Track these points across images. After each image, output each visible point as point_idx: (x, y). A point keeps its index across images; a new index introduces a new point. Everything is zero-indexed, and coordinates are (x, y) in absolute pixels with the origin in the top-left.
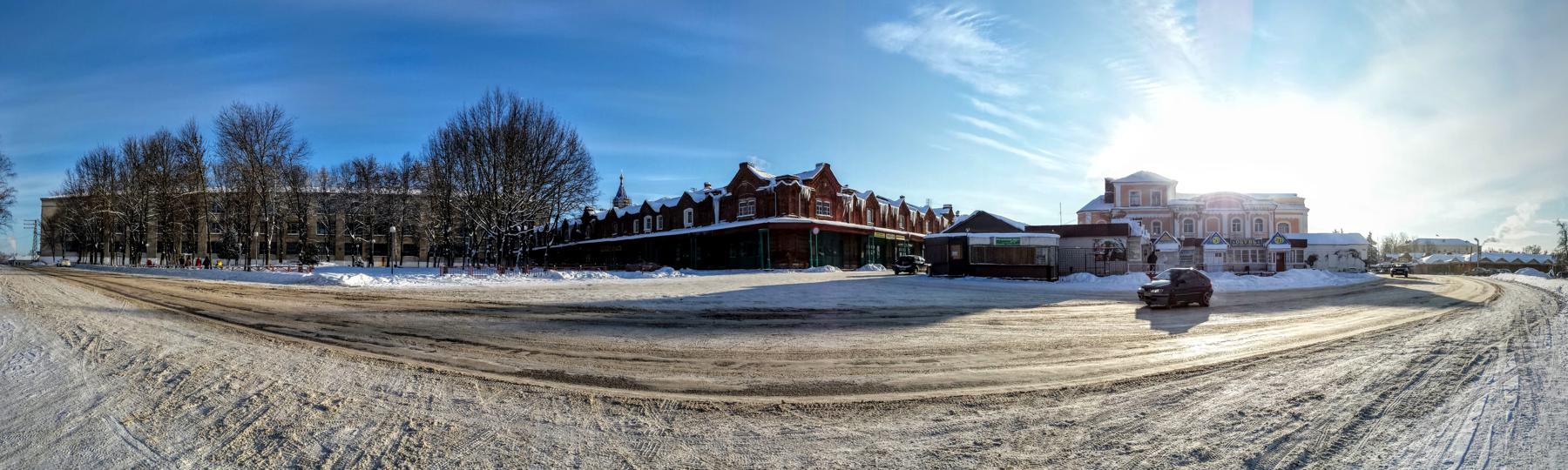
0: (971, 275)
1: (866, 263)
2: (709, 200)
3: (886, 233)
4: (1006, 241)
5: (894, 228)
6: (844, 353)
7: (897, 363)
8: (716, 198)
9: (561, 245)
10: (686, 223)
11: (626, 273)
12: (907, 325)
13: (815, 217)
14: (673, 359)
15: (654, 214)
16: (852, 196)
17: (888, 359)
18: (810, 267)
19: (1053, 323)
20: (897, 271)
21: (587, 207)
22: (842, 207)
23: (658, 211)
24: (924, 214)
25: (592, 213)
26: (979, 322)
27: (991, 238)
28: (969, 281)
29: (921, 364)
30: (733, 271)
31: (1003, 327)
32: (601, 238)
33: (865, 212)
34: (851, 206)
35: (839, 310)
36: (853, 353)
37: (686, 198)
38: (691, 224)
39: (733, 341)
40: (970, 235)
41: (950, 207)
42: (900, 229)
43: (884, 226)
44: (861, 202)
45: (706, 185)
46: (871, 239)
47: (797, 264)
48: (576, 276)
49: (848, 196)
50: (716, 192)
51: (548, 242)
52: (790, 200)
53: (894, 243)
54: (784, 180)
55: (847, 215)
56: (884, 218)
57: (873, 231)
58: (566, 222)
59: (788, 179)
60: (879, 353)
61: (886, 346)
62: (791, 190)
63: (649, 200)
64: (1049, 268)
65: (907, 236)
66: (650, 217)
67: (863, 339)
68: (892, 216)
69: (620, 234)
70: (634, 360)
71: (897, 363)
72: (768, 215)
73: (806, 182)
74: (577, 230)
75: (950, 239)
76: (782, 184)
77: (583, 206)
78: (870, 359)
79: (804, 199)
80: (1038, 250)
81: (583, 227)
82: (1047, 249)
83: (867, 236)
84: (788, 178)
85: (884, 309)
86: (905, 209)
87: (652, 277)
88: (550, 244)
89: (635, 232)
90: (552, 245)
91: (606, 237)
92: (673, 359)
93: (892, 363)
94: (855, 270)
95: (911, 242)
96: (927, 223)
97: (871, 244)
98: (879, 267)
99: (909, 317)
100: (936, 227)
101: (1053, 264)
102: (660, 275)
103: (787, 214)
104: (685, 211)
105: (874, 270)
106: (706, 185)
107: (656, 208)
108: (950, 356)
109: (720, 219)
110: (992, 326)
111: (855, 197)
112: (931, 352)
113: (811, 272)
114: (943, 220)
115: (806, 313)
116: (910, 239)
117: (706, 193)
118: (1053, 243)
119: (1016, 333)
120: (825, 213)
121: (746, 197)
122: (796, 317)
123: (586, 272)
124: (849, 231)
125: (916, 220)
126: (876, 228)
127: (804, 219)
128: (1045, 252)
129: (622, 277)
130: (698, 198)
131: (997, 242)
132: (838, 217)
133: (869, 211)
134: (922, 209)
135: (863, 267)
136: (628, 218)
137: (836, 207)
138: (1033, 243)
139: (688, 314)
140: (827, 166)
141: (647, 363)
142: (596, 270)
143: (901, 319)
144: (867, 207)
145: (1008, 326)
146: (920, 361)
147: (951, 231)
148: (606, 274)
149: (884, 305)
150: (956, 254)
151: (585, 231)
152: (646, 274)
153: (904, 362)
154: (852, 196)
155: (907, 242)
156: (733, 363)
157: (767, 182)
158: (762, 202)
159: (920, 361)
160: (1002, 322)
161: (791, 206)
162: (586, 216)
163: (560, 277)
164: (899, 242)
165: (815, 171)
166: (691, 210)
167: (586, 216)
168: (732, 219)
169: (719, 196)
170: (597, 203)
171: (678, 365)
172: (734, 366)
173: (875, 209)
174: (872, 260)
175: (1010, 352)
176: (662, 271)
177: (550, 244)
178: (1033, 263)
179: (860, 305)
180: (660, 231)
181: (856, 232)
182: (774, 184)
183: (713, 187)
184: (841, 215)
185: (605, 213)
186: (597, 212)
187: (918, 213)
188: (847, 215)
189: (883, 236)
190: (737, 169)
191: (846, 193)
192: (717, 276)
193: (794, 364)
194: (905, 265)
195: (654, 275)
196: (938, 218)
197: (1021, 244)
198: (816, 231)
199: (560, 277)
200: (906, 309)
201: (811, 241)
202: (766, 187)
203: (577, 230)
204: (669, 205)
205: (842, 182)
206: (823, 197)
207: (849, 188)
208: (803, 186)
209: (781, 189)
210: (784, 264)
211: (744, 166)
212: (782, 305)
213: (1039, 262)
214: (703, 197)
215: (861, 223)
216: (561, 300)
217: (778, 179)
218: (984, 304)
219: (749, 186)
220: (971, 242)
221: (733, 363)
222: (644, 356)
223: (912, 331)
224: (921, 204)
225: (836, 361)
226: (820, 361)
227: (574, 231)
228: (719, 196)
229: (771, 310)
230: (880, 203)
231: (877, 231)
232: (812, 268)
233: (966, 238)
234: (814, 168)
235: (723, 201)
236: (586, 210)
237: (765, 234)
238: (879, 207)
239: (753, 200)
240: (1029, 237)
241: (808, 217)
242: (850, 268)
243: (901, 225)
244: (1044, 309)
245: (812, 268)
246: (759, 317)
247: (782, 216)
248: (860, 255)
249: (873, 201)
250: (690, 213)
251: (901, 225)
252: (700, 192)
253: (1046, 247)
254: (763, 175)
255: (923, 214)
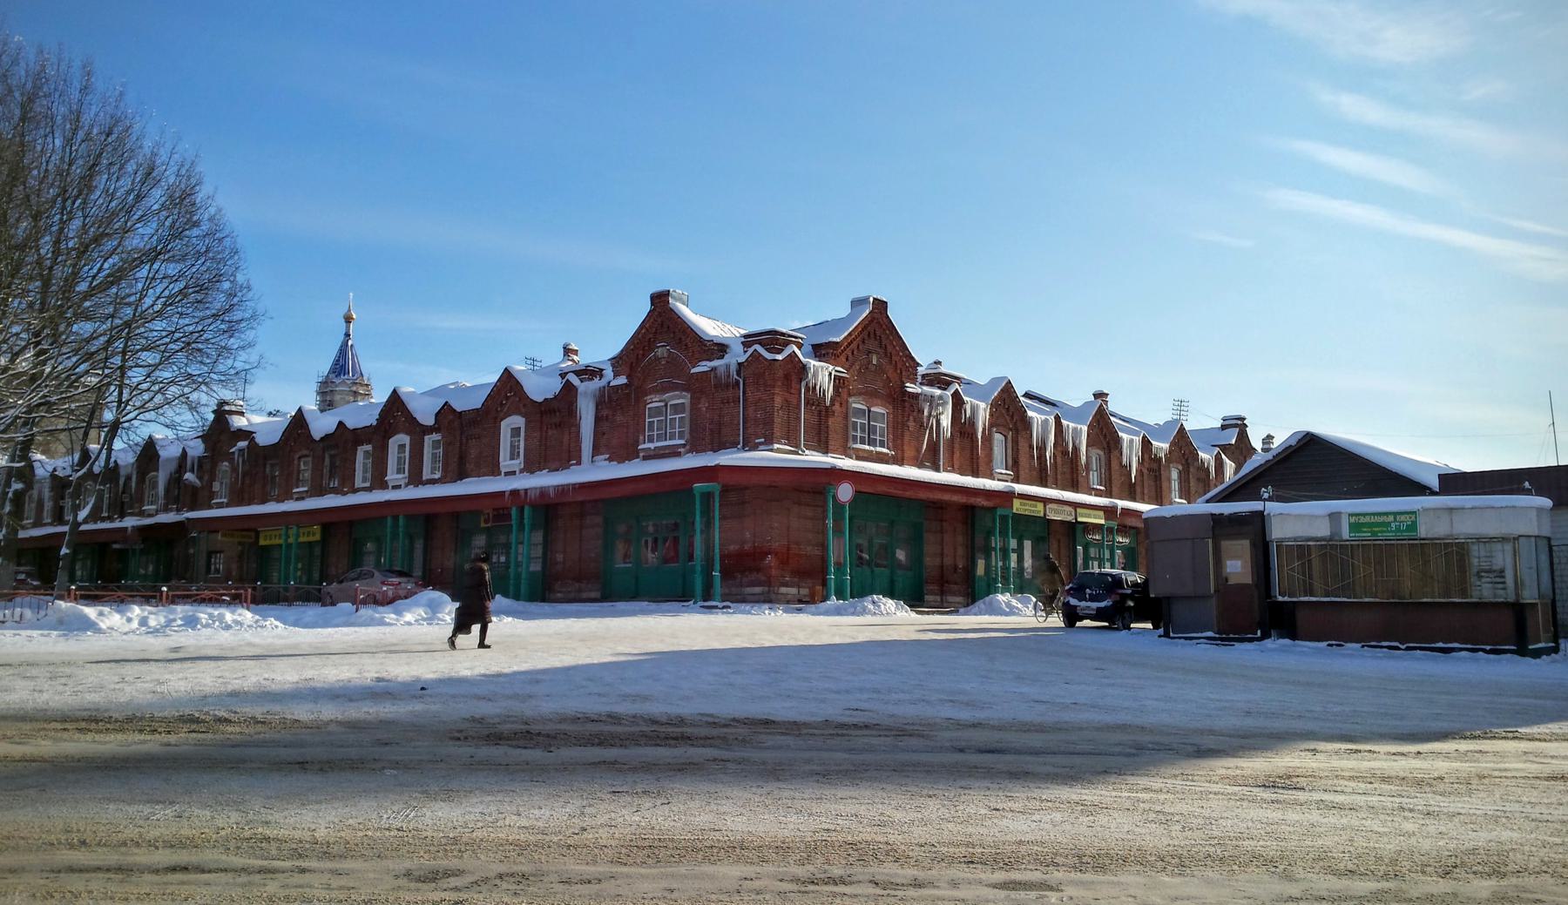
0: (1281, 636)
1: (990, 589)
2: (568, 390)
3: (1045, 501)
4: (1379, 521)
5: (1075, 487)
6: (783, 849)
7: (931, 884)
8: (587, 391)
9: (130, 522)
10: (506, 463)
11: (313, 611)
12: (1020, 775)
13: (846, 452)
14: (288, 864)
15: (418, 431)
16: (949, 393)
17: (910, 872)
18: (825, 598)
19: (1470, 793)
20: (1071, 617)
21: (222, 403)
22: (922, 427)
23: (428, 420)
24: (1165, 446)
25: (239, 422)
26: (1234, 781)
27: (1334, 517)
28: (1275, 654)
29: (1002, 894)
30: (621, 605)
31: (1302, 796)
32: (264, 502)
33: (988, 439)
34: (946, 421)
35: (842, 726)
36: (812, 850)
37: (508, 387)
38: (518, 464)
39: (493, 808)
40: (1273, 508)
41: (1237, 424)
42: (1090, 491)
43: (1043, 483)
44: (974, 409)
45: (567, 351)
46: (1004, 518)
47: (793, 591)
48: (143, 622)
49: (938, 392)
50: (589, 373)
51: (76, 509)
52: (778, 400)
53: (1073, 530)
54: (760, 343)
55: (934, 448)
56: (1042, 457)
57: (1009, 496)
58: (149, 451)
59: (776, 341)
60: (895, 855)
61: (919, 834)
62: (780, 373)
63: (406, 389)
64: (1519, 611)
65: (1109, 512)
66: (404, 438)
67: (862, 810)
68: (1065, 453)
69: (319, 491)
70: (174, 869)
71: (931, 884)
72: (718, 446)
73: (821, 351)
74: (188, 476)
75: (1217, 519)
76: (756, 356)
77: (207, 402)
78: (857, 869)
79: (815, 400)
80: (1476, 551)
81: (206, 466)
82: (1508, 547)
83: (993, 509)
84: (774, 340)
85: (975, 725)
86: (1103, 428)
87: (382, 623)
88: (82, 515)
89: (358, 483)
90: (90, 519)
91: (279, 500)
92: (288, 864)
93: (917, 884)
94: (956, 612)
95: (1123, 529)
96: (1175, 475)
97: (1004, 534)
98: (1025, 602)
99: (1036, 752)
100: (1196, 478)
101: (1529, 596)
102: (409, 617)
103: (769, 441)
104: (503, 424)
105: (1012, 611)
106: (567, 351)
107: (425, 413)
108: (1101, 878)
109: (596, 450)
110: (1267, 795)
111: (957, 397)
112: (1049, 861)
113: (827, 613)
114: (1220, 465)
115: (742, 731)
116: (1122, 522)
117: (563, 375)
118: (1529, 526)
119: (1333, 819)
120: (872, 442)
121: (665, 389)
122: (706, 741)
123: (181, 610)
124: (938, 496)
125: (1141, 463)
126: (1020, 488)
127: (814, 458)
128: (1502, 558)
129: (296, 624)
130: (540, 388)
131: (1355, 527)
132: (909, 452)
133: (998, 438)
134: (1160, 431)
135: (980, 604)
136: (343, 438)
137: (904, 425)
138: (1465, 527)
139: (414, 730)
140: (881, 306)
141: (206, 876)
142: (215, 601)
143: (1009, 758)
144: (994, 423)
145: (1317, 796)
146: (1004, 886)
147: (1230, 495)
148: (246, 615)
149: (980, 715)
150: (1237, 567)
151: (212, 479)
152: (365, 612)
153: (954, 884)
154: (949, 393)
155: (1110, 530)
156: (458, 873)
157: (720, 349)
158: (703, 405)
159: (1004, 886)
160: (1303, 782)
161: (779, 418)
162: (220, 432)
163: (88, 625)
164: (1088, 527)
165: (850, 318)
166: (517, 421)
167: (220, 432)
168: (627, 452)
169: (596, 384)
170: (252, 391)
171: (298, 879)
172: (454, 882)
173: (1016, 431)
174: (1005, 579)
175: (1288, 877)
176: (418, 605)
177: (82, 515)
178: (1464, 593)
179: (909, 711)
180: (433, 482)
181: (956, 498)
182: (737, 355)
183: (583, 359)
184: (918, 450)
185: (282, 423)
186: (258, 419)
187: (1146, 444)
188: (934, 448)
189: (1038, 510)
190: (646, 307)
191: (931, 384)
192: (570, 622)
193: (628, 876)
194: (1093, 599)
195: (390, 617)
196: (1206, 456)
197: (1423, 531)
198: (845, 492)
199: (90, 625)
200: (1041, 729)
201: (830, 523)
202: (716, 363)
203: (188, 476)
204: (459, 406)
205: (924, 358)
206: (870, 395)
207: (943, 369)
208: (813, 363)
209: (755, 370)
210: (758, 590)
211: (660, 300)
212: (686, 709)
213: (1484, 591)
214: (555, 386)
215: (976, 474)
216: (45, 696)
217: (749, 340)
218: (1278, 725)
219: (671, 360)
220: (1277, 531)
221: (458, 873)
222: (209, 856)
223: (1021, 797)
224: (1157, 414)
225: (749, 870)
226: (708, 869)
227: (176, 479)
228: (596, 384)
229: (654, 722)
230: (1030, 413)
231: (1023, 496)
232: (833, 601)
233: (1260, 516)
234: (843, 310)
235: (608, 402)
236: (222, 413)
237: (707, 497)
238: (1026, 424)
239: (683, 399)
240: (1451, 510)
241: (826, 451)
242: (941, 607)
243: (1094, 479)
244: (1464, 746)
245: (833, 601)
246: (601, 741)
247: (755, 448)
248: (974, 564)
249: (1008, 407)
250: (402, 447)
251: (1094, 479)
252: (545, 372)
253: (1504, 539)
254: (710, 328)
255: (1161, 446)
